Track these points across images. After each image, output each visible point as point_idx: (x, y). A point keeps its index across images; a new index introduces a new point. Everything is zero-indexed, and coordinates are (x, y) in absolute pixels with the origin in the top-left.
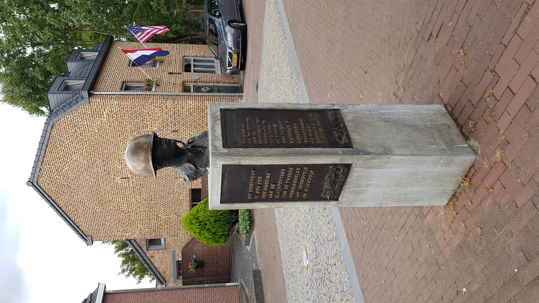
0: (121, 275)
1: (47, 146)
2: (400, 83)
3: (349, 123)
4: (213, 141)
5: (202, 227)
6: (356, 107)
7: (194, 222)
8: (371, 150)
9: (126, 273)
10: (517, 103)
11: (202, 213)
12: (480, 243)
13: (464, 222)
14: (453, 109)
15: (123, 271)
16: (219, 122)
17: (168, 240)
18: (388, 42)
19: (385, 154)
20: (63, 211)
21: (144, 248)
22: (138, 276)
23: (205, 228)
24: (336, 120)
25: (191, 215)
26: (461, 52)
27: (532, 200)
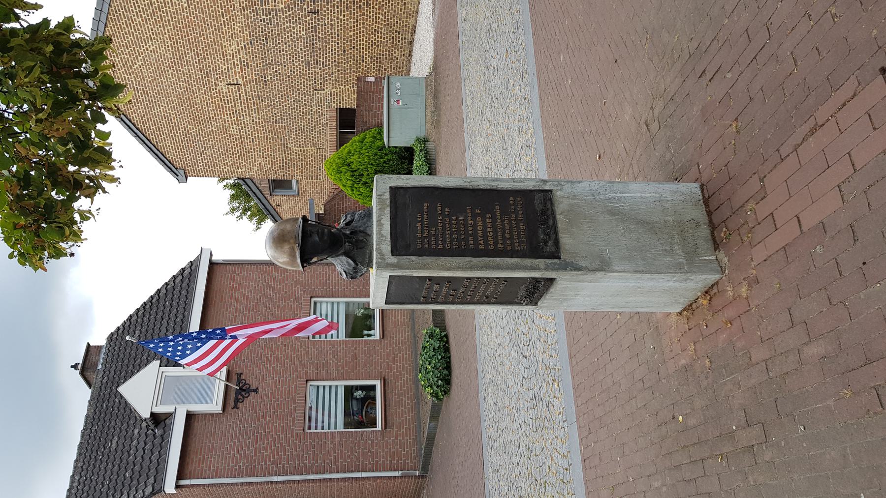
0: (230, 215)
1: (106, 26)
2: (656, 112)
3: (561, 217)
4: (379, 244)
5: (356, 178)
6: (578, 187)
7: (343, 169)
8: (583, 263)
9: (238, 214)
10: (776, 241)
11: (356, 157)
12: (707, 378)
13: (695, 343)
14: (709, 197)
15: (233, 210)
16: (387, 211)
17: (303, 183)
18: (651, 38)
19: (601, 269)
20: (137, 129)
21: (267, 192)
22: (255, 220)
23: (361, 180)
24: (544, 212)
25: (339, 158)
26: (734, 125)
27: (766, 361)
